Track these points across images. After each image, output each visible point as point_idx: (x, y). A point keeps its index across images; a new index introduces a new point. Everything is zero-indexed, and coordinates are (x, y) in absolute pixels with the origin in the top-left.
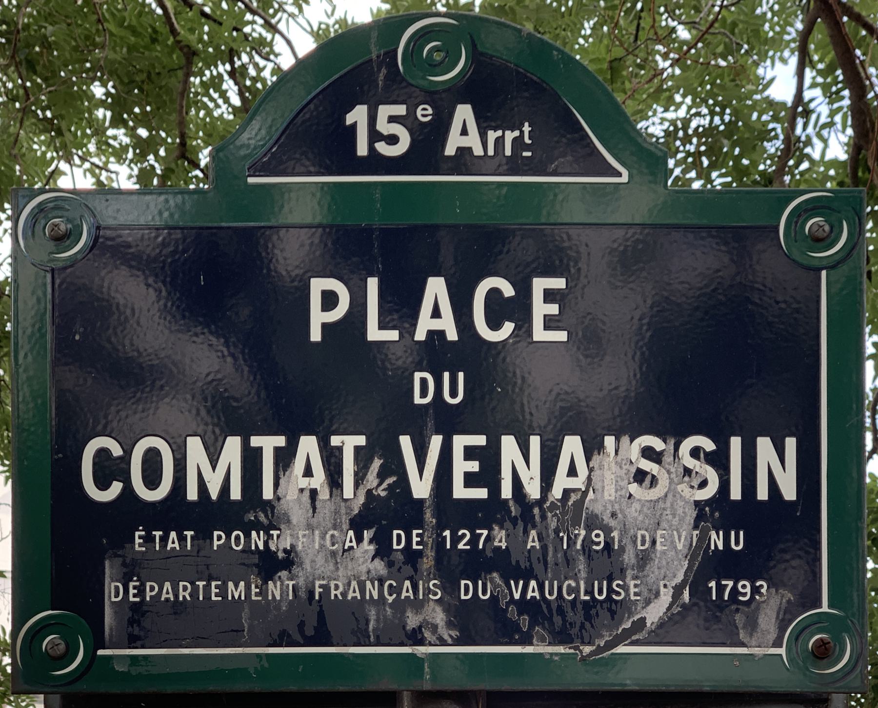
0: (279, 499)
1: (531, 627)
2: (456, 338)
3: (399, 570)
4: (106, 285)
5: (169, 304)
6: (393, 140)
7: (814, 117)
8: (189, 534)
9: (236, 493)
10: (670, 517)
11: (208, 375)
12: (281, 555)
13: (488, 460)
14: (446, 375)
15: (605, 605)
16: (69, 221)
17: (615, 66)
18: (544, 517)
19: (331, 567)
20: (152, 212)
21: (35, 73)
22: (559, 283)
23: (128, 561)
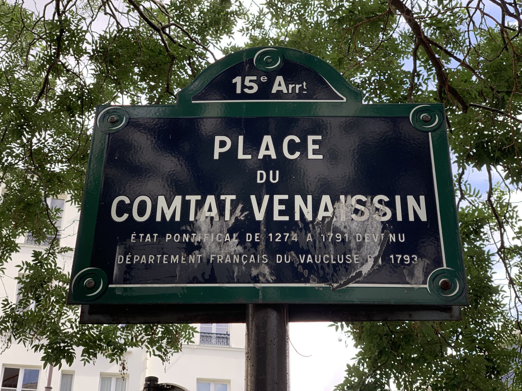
0: (196, 221)
1: (309, 275)
2: (275, 158)
3: (249, 250)
4: (130, 139)
5: (156, 146)
6: (251, 88)
7: (421, 77)
8: (155, 235)
9: (178, 218)
10: (371, 228)
11: (169, 172)
12: (196, 244)
13: (289, 205)
14: (271, 172)
15: (343, 266)
16: (118, 116)
17: (340, 61)
18: (314, 228)
19: (218, 249)
20: (154, 113)
21: (113, 65)
22: (319, 137)
23: (127, 246)
